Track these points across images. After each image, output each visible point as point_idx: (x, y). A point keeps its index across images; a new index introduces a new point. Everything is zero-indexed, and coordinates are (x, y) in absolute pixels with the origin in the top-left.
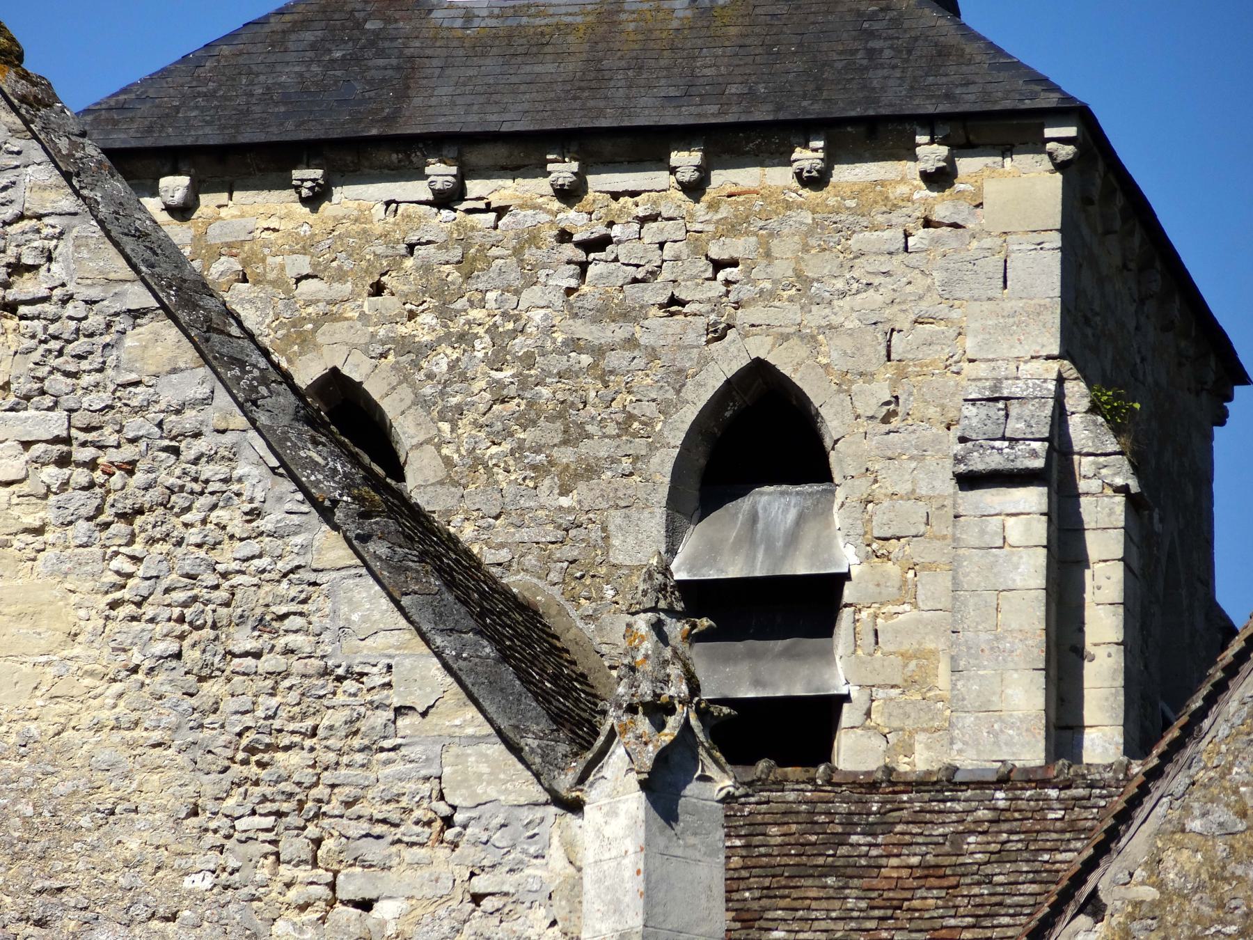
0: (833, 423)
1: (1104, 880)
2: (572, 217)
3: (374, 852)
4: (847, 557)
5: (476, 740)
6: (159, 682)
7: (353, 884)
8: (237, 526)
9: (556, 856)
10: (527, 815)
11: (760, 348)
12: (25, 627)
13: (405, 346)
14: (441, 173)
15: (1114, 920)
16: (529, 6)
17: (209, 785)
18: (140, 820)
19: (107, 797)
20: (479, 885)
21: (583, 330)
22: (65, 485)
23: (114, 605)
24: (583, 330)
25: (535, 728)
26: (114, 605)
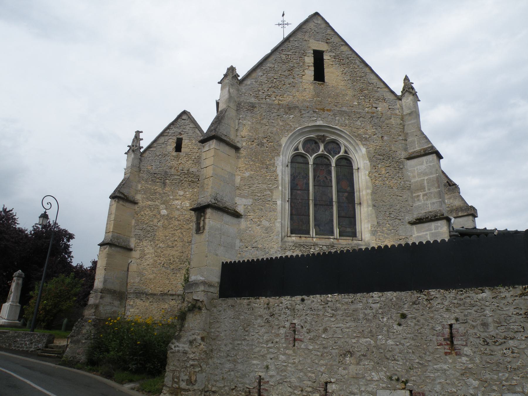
3: (377, 102)
5: (387, 92)
6: (349, 82)
7: (374, 105)
8: (356, 67)
9: (398, 106)
10: (395, 100)
12: (332, 74)
17: (356, 93)
18: (348, 96)
19: (343, 93)
20: (390, 107)
22: (335, 61)
23: (342, 73)
26: (342, 73)
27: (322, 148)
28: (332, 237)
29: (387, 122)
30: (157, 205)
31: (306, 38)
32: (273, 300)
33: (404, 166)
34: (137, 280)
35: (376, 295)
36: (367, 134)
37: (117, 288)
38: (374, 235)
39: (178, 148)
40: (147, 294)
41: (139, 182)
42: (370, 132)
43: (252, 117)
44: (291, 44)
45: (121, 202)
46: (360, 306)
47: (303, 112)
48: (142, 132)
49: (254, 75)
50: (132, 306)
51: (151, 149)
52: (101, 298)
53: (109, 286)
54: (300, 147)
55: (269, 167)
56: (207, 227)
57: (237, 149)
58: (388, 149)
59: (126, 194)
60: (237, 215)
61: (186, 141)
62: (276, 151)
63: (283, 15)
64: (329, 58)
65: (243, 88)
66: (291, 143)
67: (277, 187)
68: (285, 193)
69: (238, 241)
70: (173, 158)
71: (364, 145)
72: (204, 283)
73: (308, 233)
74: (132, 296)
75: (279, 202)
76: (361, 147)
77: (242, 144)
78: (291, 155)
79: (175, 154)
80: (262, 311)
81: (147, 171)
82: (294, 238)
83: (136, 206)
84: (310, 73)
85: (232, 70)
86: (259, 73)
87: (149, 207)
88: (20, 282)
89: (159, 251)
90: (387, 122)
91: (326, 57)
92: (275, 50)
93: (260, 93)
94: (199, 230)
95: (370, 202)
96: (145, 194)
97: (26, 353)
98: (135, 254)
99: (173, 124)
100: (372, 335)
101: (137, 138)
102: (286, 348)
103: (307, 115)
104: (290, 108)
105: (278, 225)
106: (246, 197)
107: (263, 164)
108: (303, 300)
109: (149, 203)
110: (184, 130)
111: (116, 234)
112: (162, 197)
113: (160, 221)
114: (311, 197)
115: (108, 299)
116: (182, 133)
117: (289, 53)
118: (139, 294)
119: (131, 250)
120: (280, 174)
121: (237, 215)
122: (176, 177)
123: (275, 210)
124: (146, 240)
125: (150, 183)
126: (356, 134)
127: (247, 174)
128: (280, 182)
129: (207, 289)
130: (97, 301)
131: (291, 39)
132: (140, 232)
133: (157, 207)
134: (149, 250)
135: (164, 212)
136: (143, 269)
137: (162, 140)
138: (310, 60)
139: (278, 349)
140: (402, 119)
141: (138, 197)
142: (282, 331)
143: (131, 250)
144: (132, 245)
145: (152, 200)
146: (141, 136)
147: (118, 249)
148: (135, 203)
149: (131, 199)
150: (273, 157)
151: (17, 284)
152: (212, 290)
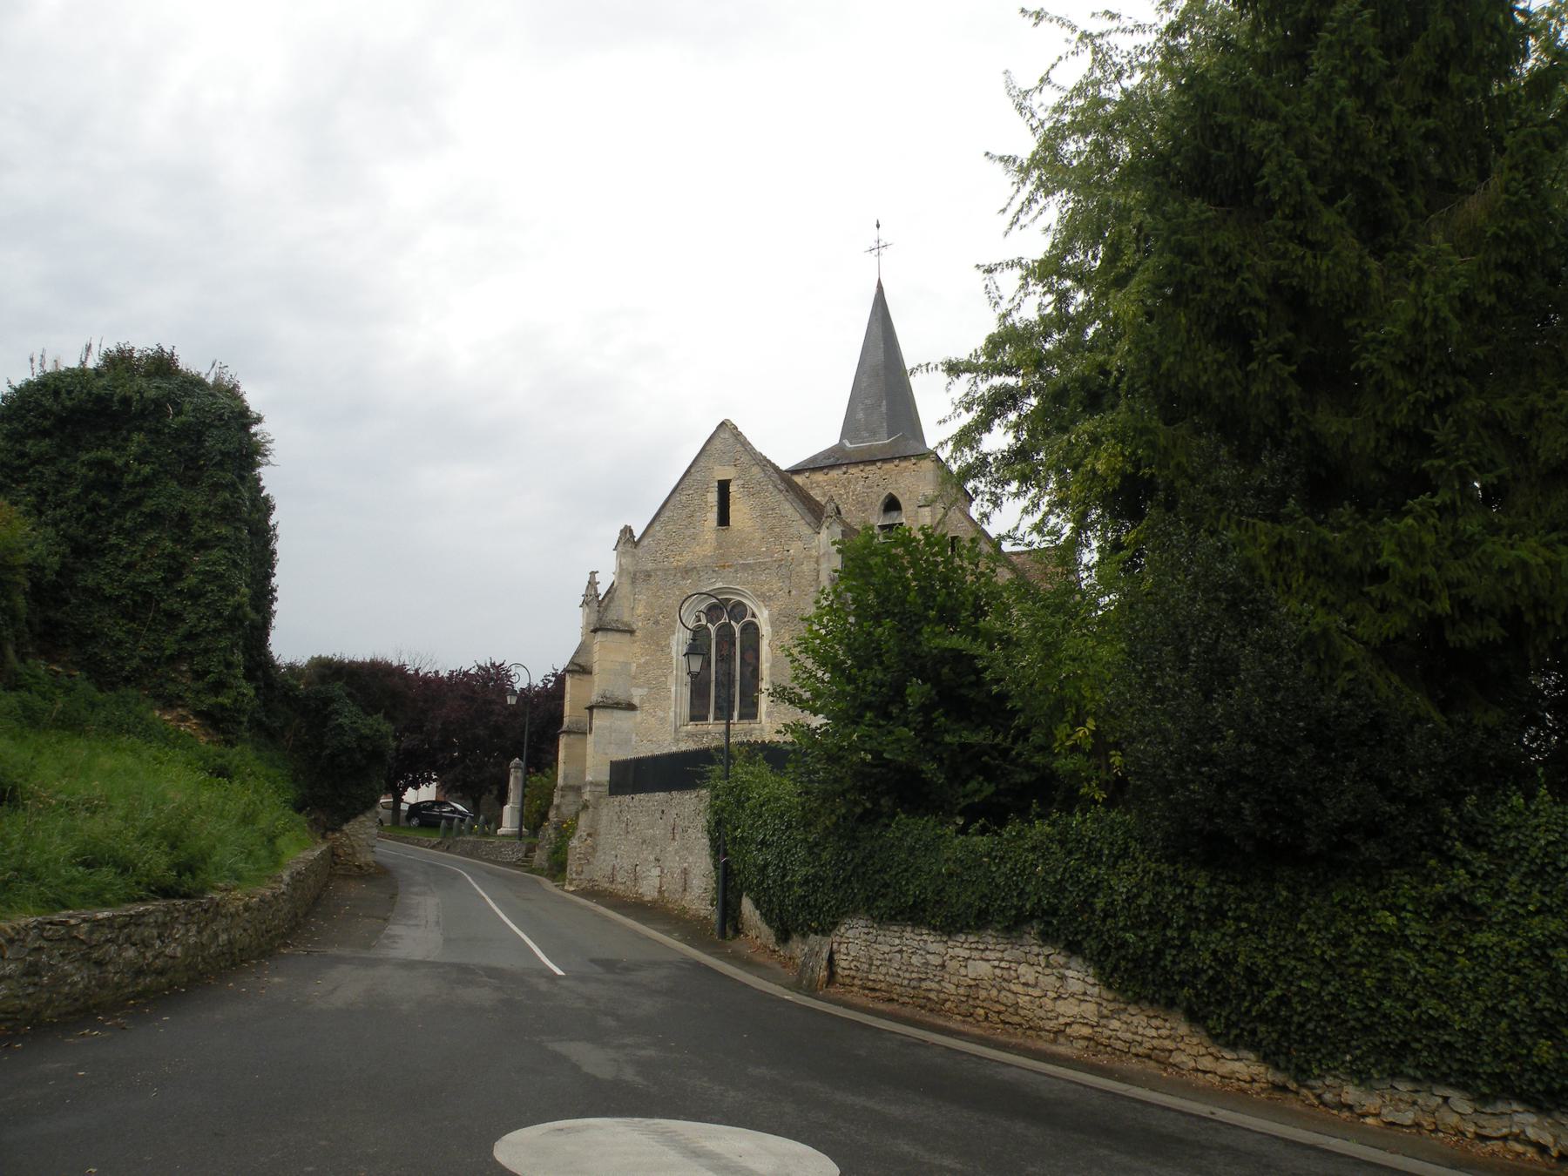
14: (844, 469)
29: (798, 569)
31: (710, 465)
42: (775, 587)
45: (577, 676)
49: (651, 531)
55: (664, 648)
57: (632, 632)
60: (631, 707)
63: (878, 226)
65: (639, 551)
75: (673, 689)
77: (638, 625)
84: (713, 516)
85: (627, 531)
86: (657, 527)
88: (520, 774)
90: (798, 569)
97: (508, 864)
104: (687, 571)
105: (672, 714)
107: (658, 645)
114: (713, 678)
121: (631, 707)
123: (669, 698)
129: (593, 788)
138: (713, 497)
140: (817, 562)
146: (598, 578)
151: (516, 777)
152: (599, 789)
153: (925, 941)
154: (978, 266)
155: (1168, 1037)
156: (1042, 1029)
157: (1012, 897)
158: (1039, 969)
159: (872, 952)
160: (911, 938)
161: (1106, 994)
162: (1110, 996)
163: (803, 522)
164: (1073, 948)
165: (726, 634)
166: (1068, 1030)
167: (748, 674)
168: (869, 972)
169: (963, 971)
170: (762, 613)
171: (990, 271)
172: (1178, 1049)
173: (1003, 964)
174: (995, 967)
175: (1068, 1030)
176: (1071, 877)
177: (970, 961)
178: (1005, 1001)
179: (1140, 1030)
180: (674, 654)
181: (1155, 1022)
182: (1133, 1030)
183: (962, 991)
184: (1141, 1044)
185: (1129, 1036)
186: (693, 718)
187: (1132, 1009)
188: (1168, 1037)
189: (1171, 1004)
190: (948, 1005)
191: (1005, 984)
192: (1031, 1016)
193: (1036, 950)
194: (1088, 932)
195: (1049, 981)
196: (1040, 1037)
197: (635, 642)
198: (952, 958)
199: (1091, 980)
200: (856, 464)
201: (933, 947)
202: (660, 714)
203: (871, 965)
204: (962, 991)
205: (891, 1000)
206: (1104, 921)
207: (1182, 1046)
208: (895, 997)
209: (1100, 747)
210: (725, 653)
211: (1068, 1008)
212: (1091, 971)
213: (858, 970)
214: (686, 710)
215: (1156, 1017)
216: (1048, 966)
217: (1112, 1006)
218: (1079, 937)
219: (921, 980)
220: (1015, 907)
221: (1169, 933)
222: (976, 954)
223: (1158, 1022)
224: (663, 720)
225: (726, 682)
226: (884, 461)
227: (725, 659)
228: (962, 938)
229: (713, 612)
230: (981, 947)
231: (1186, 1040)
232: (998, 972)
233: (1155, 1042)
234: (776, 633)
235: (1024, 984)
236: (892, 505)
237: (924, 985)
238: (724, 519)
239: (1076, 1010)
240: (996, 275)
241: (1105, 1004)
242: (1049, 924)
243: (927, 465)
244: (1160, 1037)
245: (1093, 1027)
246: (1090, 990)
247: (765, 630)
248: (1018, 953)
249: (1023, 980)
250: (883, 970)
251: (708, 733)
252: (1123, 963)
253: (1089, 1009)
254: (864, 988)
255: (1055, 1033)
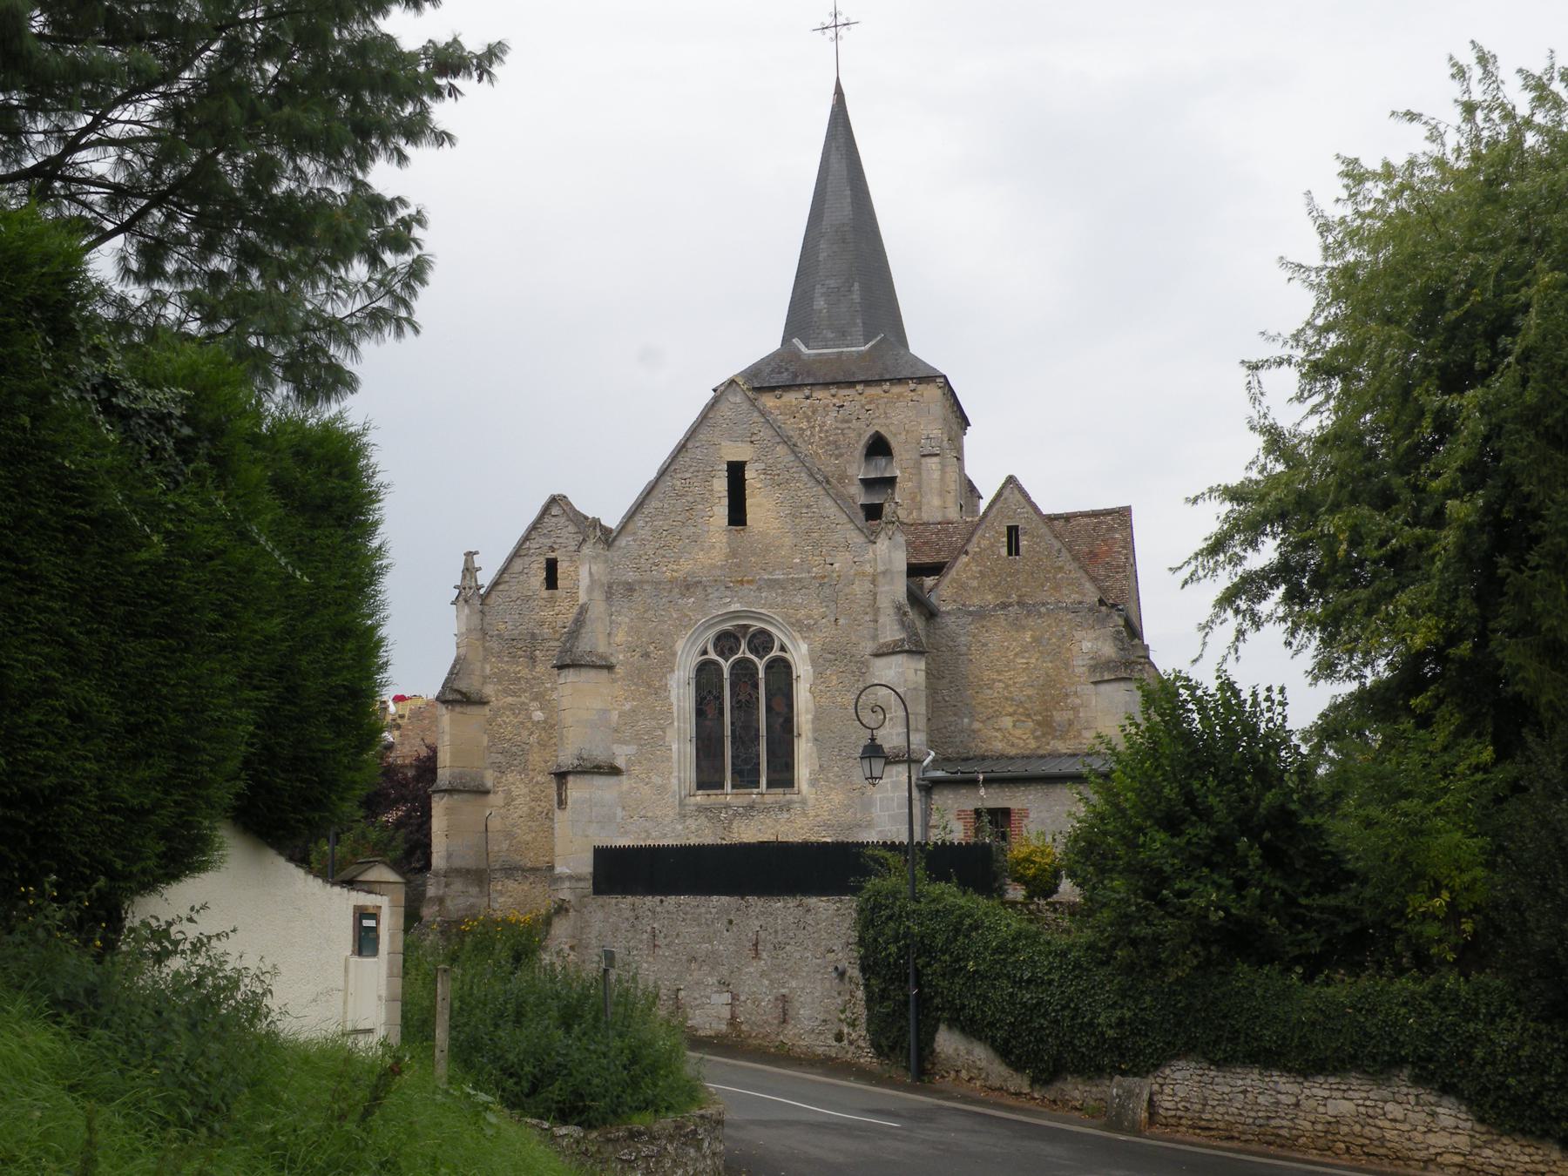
0: (894, 443)
1: (969, 548)
2: (835, 401)
4: (898, 473)
7: (829, 560)
11: (877, 428)
13: (801, 429)
14: (807, 392)
15: (971, 555)
16: (1249, 389)
19: (777, 544)
21: (839, 425)
24: (839, 425)
25: (344, 104)
27: (743, 646)
28: (755, 791)
29: (847, 590)
30: (524, 703)
31: (716, 440)
32: (638, 900)
33: (868, 667)
34: (505, 846)
35: (715, 898)
36: (812, 618)
37: (469, 862)
38: (813, 786)
39: (551, 581)
40: (523, 870)
41: (485, 659)
43: (630, 608)
44: (689, 455)
45: (458, 709)
46: (703, 910)
47: (709, 590)
48: (476, 553)
49: (630, 527)
50: (501, 893)
51: (501, 587)
52: (447, 885)
53: (458, 863)
54: (710, 649)
55: (660, 691)
56: (569, 801)
57: (610, 668)
58: (844, 640)
59: (464, 690)
60: (614, 771)
61: (565, 564)
62: (668, 664)
64: (755, 475)
65: (613, 554)
66: (693, 644)
67: (672, 723)
68: (685, 730)
69: (619, 810)
70: (542, 603)
71: (804, 638)
72: (570, 877)
73: (722, 786)
74: (498, 875)
75: (675, 747)
76: (801, 642)
78: (694, 664)
79: (545, 593)
80: (628, 914)
81: (498, 635)
82: (700, 798)
83: (487, 708)
84: (722, 511)
86: (639, 521)
87: (511, 707)
89: (537, 789)
90: (847, 590)
91: (749, 474)
92: (663, 473)
93: (643, 561)
94: (562, 803)
95: (810, 735)
96: (499, 682)
98: (496, 799)
99: (534, 527)
100: (710, 942)
101: (469, 570)
102: (648, 955)
103: (716, 594)
104: (688, 586)
105: (674, 781)
106: (625, 743)
107: (649, 686)
108: (662, 901)
109: (510, 700)
110: (559, 541)
111: (457, 770)
112: (532, 687)
113: (532, 733)
115: (458, 886)
116: (556, 546)
117: (688, 475)
118: (510, 871)
119: (487, 792)
120: (675, 702)
121: (614, 771)
122: (551, 643)
123: (669, 759)
124: (512, 771)
125: (506, 659)
126: (793, 620)
127: (627, 707)
128: (675, 715)
129: (574, 884)
130: (441, 892)
131: (690, 445)
132: (500, 758)
133: (524, 707)
134: (520, 790)
135: (538, 715)
136: (513, 825)
137: (518, 565)
138: (721, 485)
139: (641, 956)
140: (873, 582)
141: (489, 690)
142: (645, 936)
143: (487, 792)
144: (489, 784)
145: (514, 694)
146: (478, 561)
147: (465, 796)
148: (482, 702)
149: (474, 697)
150: (664, 675)
152: (582, 884)
153: (1276, 1083)
154: (1243, 362)
155: (1541, 1162)
156: (1409, 1159)
157: (1384, 1044)
158: (1409, 1107)
159: (1207, 1093)
160: (1251, 1079)
161: (1478, 1127)
162: (1484, 1129)
163: (851, 526)
164: (1446, 1089)
165: (744, 671)
166: (1439, 1159)
167: (777, 726)
168: (1203, 1111)
169: (1321, 1109)
170: (796, 647)
171: (1255, 367)
172: (1551, 1171)
173: (1368, 1103)
174: (1358, 1105)
175: (1439, 1159)
176: (1448, 1030)
177: (1330, 1101)
178: (1369, 1135)
179: (1514, 1157)
180: (674, 699)
181: (1527, 1150)
182: (1506, 1156)
183: (1319, 1127)
184: (1514, 1168)
185: (1502, 1162)
186: (701, 786)
187: (1505, 1140)
188: (1541, 1162)
189: (1544, 1135)
190: (1302, 1140)
191: (1370, 1121)
192: (1399, 1147)
193: (1405, 1090)
194: (1465, 1075)
195: (1419, 1117)
196: (1409, 1166)
197: (614, 681)
198: (1308, 1097)
199: (1463, 1116)
200: (826, 385)
201: (1282, 1088)
202: (657, 780)
203: (1204, 1105)
204: (1319, 1127)
205: (1232, 1138)
206: (1482, 1067)
207: (1555, 1169)
208: (1236, 1135)
209: (1454, 913)
210: (742, 697)
211: (1439, 1140)
212: (1464, 1108)
213: (1187, 1109)
214: (690, 774)
215: (1529, 1146)
216: (1417, 1104)
217: (1484, 1138)
218: (1455, 1080)
219: (1269, 1118)
220: (1389, 1054)
221: (1547, 1079)
222: (1338, 1094)
223: (1531, 1150)
224: (662, 790)
225: (745, 736)
226: (867, 383)
227: (744, 707)
228: (1321, 1079)
229: (726, 642)
230: (1343, 1087)
231: (1559, 1164)
232: (1362, 1109)
233: (1528, 1167)
234: (819, 674)
235: (1391, 1120)
236: (879, 447)
237: (1273, 1123)
238: (737, 515)
239: (1447, 1142)
240: (1262, 374)
241: (1478, 1136)
242: (1424, 1068)
243: (932, 392)
244: (1533, 1162)
245: (1464, 1155)
246: (1462, 1124)
247: (803, 669)
248: (1386, 1093)
249: (1390, 1117)
250: (1221, 1110)
251: (727, 806)
252: (1501, 1102)
253: (1462, 1141)
254: (1195, 1128)
255: (1425, 1162)
